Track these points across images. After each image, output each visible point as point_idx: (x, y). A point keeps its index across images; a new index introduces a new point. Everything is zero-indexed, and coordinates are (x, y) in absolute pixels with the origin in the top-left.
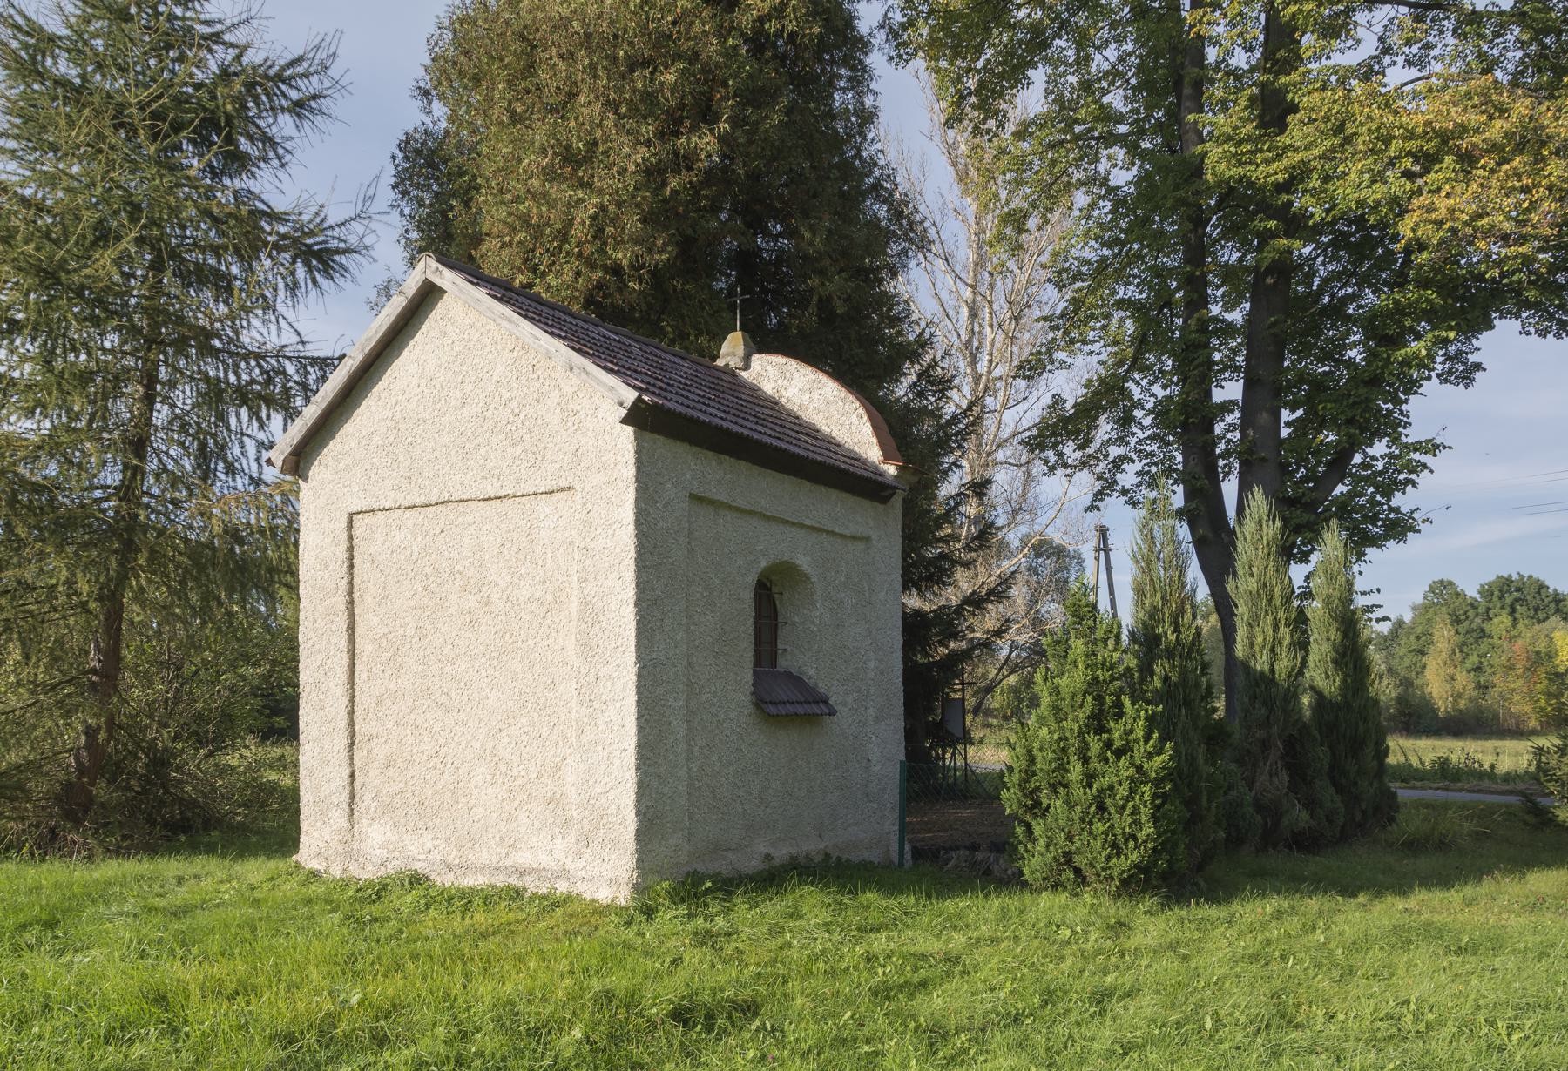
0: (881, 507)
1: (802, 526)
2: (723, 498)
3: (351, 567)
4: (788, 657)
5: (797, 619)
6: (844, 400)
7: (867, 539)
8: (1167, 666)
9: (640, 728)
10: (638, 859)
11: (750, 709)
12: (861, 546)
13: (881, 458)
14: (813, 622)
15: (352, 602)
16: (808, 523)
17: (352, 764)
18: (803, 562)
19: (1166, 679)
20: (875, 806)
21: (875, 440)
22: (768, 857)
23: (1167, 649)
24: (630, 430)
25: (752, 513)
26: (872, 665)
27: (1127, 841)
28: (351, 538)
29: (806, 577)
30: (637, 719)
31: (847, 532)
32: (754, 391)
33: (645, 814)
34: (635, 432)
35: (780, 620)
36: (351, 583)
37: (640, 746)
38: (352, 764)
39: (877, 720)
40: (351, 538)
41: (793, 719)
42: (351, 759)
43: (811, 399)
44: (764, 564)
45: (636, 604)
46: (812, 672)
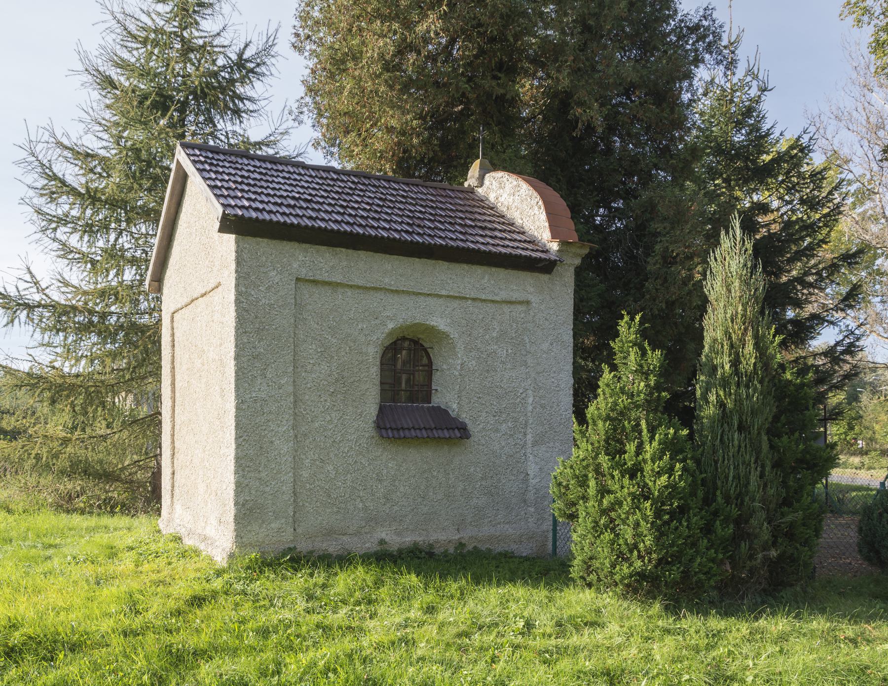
0: (545, 277)
1: (440, 296)
2: (338, 278)
3: (173, 346)
4: (439, 395)
5: (445, 367)
6: (531, 197)
7: (528, 303)
8: (721, 393)
9: (238, 446)
10: (237, 536)
11: (374, 433)
12: (520, 308)
13: (550, 237)
14: (455, 369)
15: (174, 368)
16: (444, 293)
17: (173, 466)
18: (440, 323)
19: (721, 405)
20: (532, 510)
21: (547, 224)
22: (382, 542)
23: (723, 378)
24: (230, 239)
25: (375, 289)
26: (530, 400)
27: (631, 552)
28: (173, 328)
29: (446, 336)
30: (236, 439)
31: (497, 298)
32: (482, 202)
33: (243, 505)
34: (237, 242)
35: (434, 368)
36: (173, 356)
37: (239, 460)
38: (173, 466)
39: (535, 443)
40: (173, 328)
41: (448, 440)
42: (173, 463)
43: (514, 201)
44: (391, 326)
45: (235, 359)
46: (455, 406)
